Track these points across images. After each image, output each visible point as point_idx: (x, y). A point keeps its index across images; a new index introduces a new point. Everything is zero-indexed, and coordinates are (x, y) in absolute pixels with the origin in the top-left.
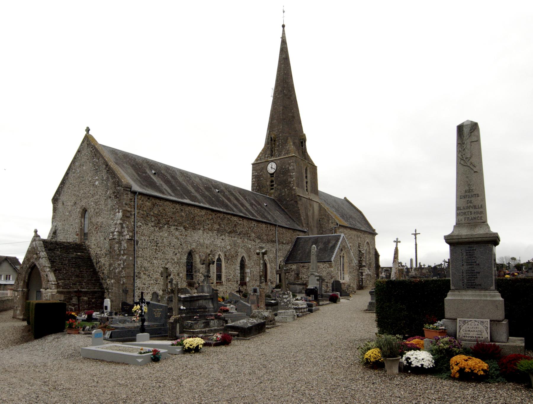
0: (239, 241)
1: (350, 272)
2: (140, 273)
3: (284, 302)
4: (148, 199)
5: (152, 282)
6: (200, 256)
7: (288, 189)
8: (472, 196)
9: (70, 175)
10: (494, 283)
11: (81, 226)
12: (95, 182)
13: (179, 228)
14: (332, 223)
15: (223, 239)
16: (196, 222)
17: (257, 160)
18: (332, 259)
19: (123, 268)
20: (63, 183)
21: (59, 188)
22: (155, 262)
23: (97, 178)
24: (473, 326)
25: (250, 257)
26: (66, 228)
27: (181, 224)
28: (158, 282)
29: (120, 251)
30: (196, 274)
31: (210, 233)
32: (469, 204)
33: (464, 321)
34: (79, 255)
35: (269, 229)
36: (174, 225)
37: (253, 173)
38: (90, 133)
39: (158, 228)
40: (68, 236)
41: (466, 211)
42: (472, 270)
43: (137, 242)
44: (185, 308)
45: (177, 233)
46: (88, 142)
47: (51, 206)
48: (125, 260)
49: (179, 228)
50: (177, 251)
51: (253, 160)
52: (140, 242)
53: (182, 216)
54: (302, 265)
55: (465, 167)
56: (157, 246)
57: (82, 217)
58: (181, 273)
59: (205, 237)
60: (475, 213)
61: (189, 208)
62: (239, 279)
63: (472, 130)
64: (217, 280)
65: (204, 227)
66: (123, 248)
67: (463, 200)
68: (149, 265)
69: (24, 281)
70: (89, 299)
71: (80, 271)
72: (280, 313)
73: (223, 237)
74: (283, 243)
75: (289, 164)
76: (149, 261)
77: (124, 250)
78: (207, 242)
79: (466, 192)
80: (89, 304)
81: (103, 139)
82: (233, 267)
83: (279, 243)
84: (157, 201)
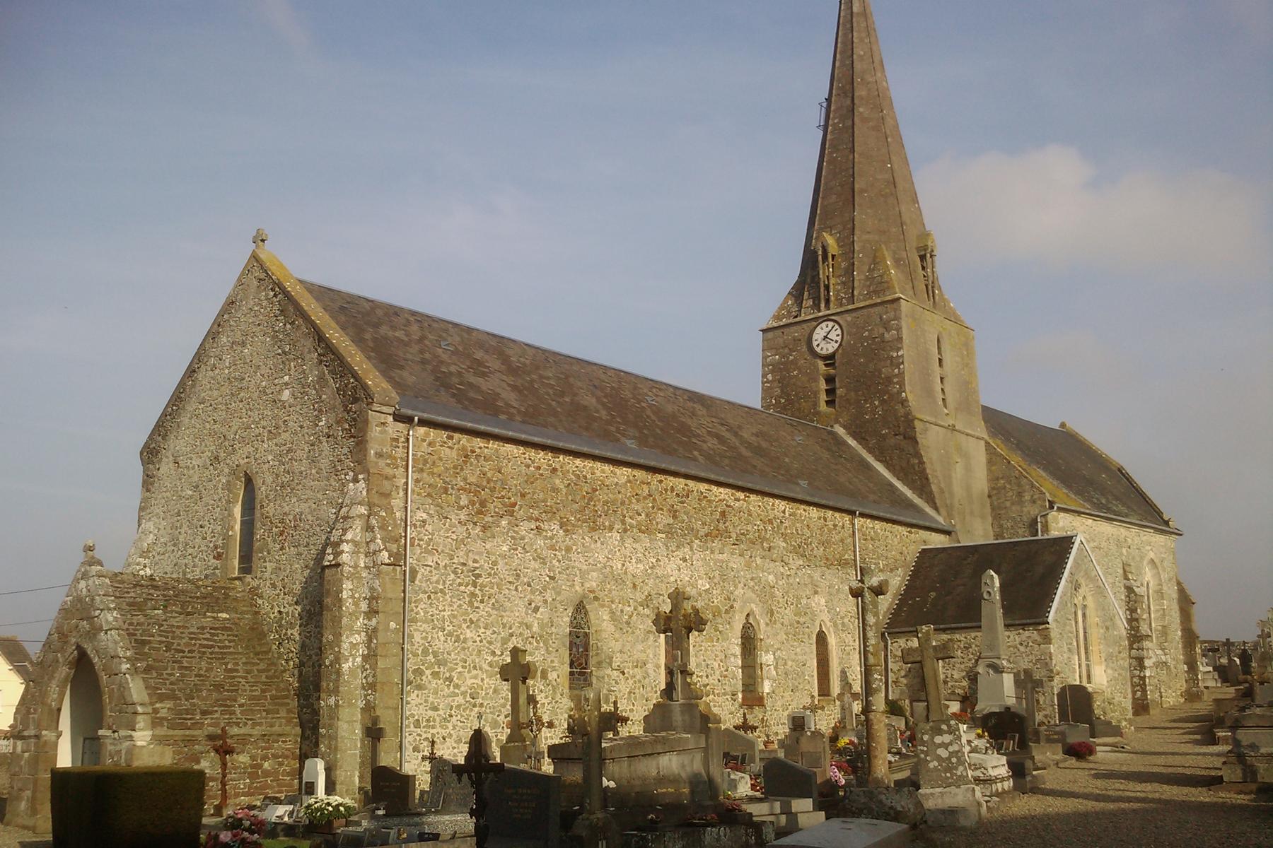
0: (736, 563)
1: (1109, 658)
3: (939, 758)
5: (460, 699)
6: (612, 613)
7: (883, 402)
12: (280, 392)
13: (545, 526)
15: (684, 560)
16: (599, 507)
20: (178, 399)
21: (164, 414)
22: (469, 634)
26: (181, 538)
27: (552, 512)
28: (479, 701)
30: (601, 673)
35: (830, 524)
36: (530, 519)
37: (765, 358)
39: (478, 529)
40: (188, 560)
43: (414, 573)
46: (260, 273)
47: (136, 470)
49: (545, 526)
50: (538, 599)
52: (422, 571)
53: (555, 490)
58: (554, 669)
61: (578, 461)
65: (623, 522)
68: (450, 646)
70: (253, 758)
71: (227, 670)
76: (450, 634)
80: (253, 776)
81: (308, 262)
82: (718, 646)
84: (478, 442)
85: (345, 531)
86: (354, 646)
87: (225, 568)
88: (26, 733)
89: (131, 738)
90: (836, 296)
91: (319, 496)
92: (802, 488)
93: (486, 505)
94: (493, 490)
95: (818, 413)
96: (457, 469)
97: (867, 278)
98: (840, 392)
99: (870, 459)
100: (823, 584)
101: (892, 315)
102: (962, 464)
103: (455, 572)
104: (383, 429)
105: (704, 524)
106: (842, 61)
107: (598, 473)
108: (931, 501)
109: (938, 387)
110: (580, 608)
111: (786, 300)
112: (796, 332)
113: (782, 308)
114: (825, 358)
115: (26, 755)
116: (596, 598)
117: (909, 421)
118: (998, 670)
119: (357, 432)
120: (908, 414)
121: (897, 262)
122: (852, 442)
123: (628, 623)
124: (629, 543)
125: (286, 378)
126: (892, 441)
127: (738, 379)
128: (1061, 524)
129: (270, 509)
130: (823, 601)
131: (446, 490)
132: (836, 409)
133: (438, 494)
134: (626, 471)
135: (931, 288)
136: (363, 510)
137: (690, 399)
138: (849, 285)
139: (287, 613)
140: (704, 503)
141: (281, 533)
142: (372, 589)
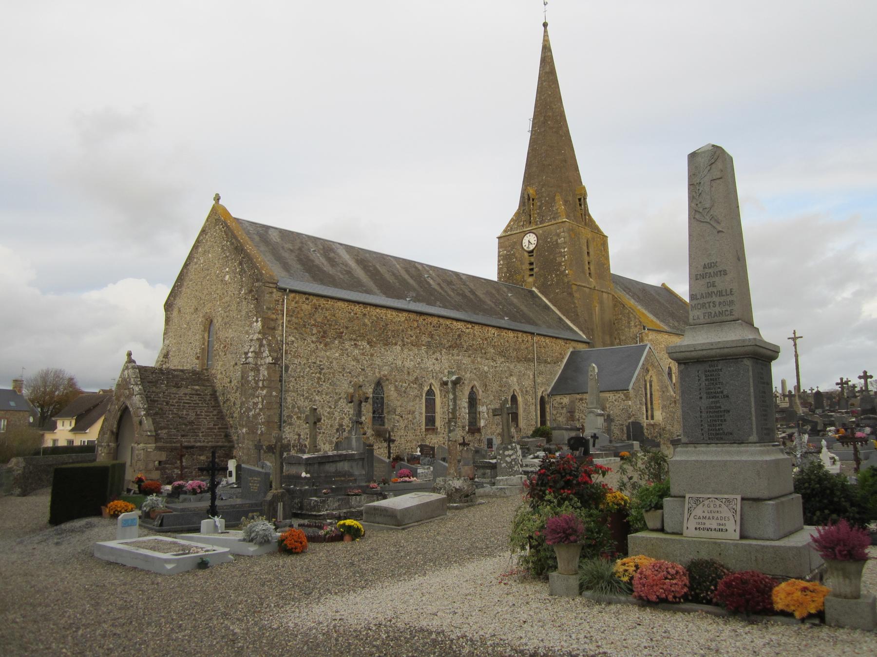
0: (466, 361)
2: (292, 417)
3: (506, 462)
4: (307, 299)
6: (396, 387)
7: (557, 275)
8: (716, 274)
9: (189, 267)
10: (754, 430)
11: (204, 344)
15: (437, 359)
16: (389, 333)
17: (505, 231)
18: (630, 387)
19: (261, 410)
22: (317, 398)
24: (712, 508)
25: (486, 386)
27: (362, 336)
29: (257, 382)
31: (416, 350)
32: (711, 289)
33: (698, 499)
34: (197, 390)
35: (520, 340)
37: (499, 252)
38: (221, 202)
41: (705, 300)
42: (717, 407)
43: (287, 367)
44: (308, 475)
45: (357, 351)
48: (265, 396)
51: (499, 232)
53: (365, 325)
54: (578, 396)
55: (702, 224)
56: (320, 373)
57: (204, 331)
60: (720, 303)
61: (378, 310)
62: (467, 423)
63: (713, 161)
64: (426, 425)
65: (403, 341)
66: (261, 378)
67: (702, 282)
69: (112, 432)
72: (499, 481)
73: (438, 355)
74: (546, 362)
75: (558, 235)
76: (307, 398)
77: (264, 380)
78: (409, 364)
79: (705, 267)
81: (244, 209)
83: (539, 363)
84: (322, 301)
96: (311, 315)
103: (309, 367)
105: (448, 341)
107: (389, 316)
109: (587, 267)
110: (379, 384)
116: (387, 380)
123: (405, 392)
124: (406, 351)
128: (650, 338)
129: (222, 335)
130: (515, 380)
131: (305, 326)
133: (300, 328)
134: (405, 314)
140: (449, 330)
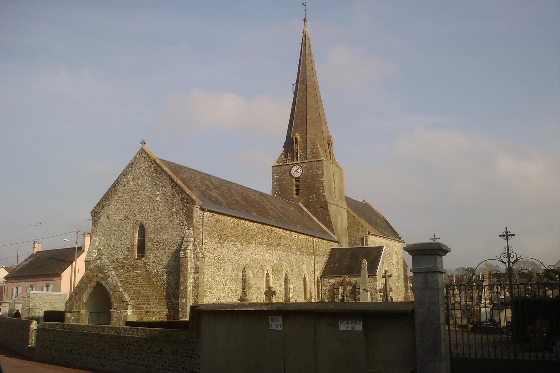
0: (284, 254)
6: (252, 271)
7: (316, 196)
13: (236, 243)
14: (363, 232)
20: (108, 195)
21: (102, 200)
23: (158, 193)
26: (112, 244)
36: (232, 241)
37: (273, 176)
46: (143, 154)
49: (236, 243)
53: (238, 231)
59: (256, 251)
71: (145, 290)
84: (220, 216)
85: (187, 246)
86: (190, 283)
87: (132, 256)
88: (73, 311)
89: (127, 312)
90: (300, 156)
91: (174, 233)
92: (299, 228)
93: (222, 237)
94: (223, 232)
95: (293, 198)
96: (215, 225)
97: (311, 151)
98: (301, 191)
99: (312, 215)
100: (306, 261)
101: (320, 165)
102: (340, 216)
104: (197, 213)
106: (302, 71)
108: (333, 231)
110: (244, 270)
111: (281, 156)
112: (285, 168)
113: (279, 158)
114: (296, 178)
115: (73, 318)
117: (326, 203)
118: (366, 291)
119: (189, 214)
120: (326, 200)
121: (321, 146)
122: (305, 209)
125: (158, 193)
126: (319, 210)
127: (263, 184)
132: (298, 195)
135: (331, 155)
136: (192, 239)
137: (260, 195)
138: (305, 153)
139: (161, 272)
141: (157, 245)
142: (196, 265)
